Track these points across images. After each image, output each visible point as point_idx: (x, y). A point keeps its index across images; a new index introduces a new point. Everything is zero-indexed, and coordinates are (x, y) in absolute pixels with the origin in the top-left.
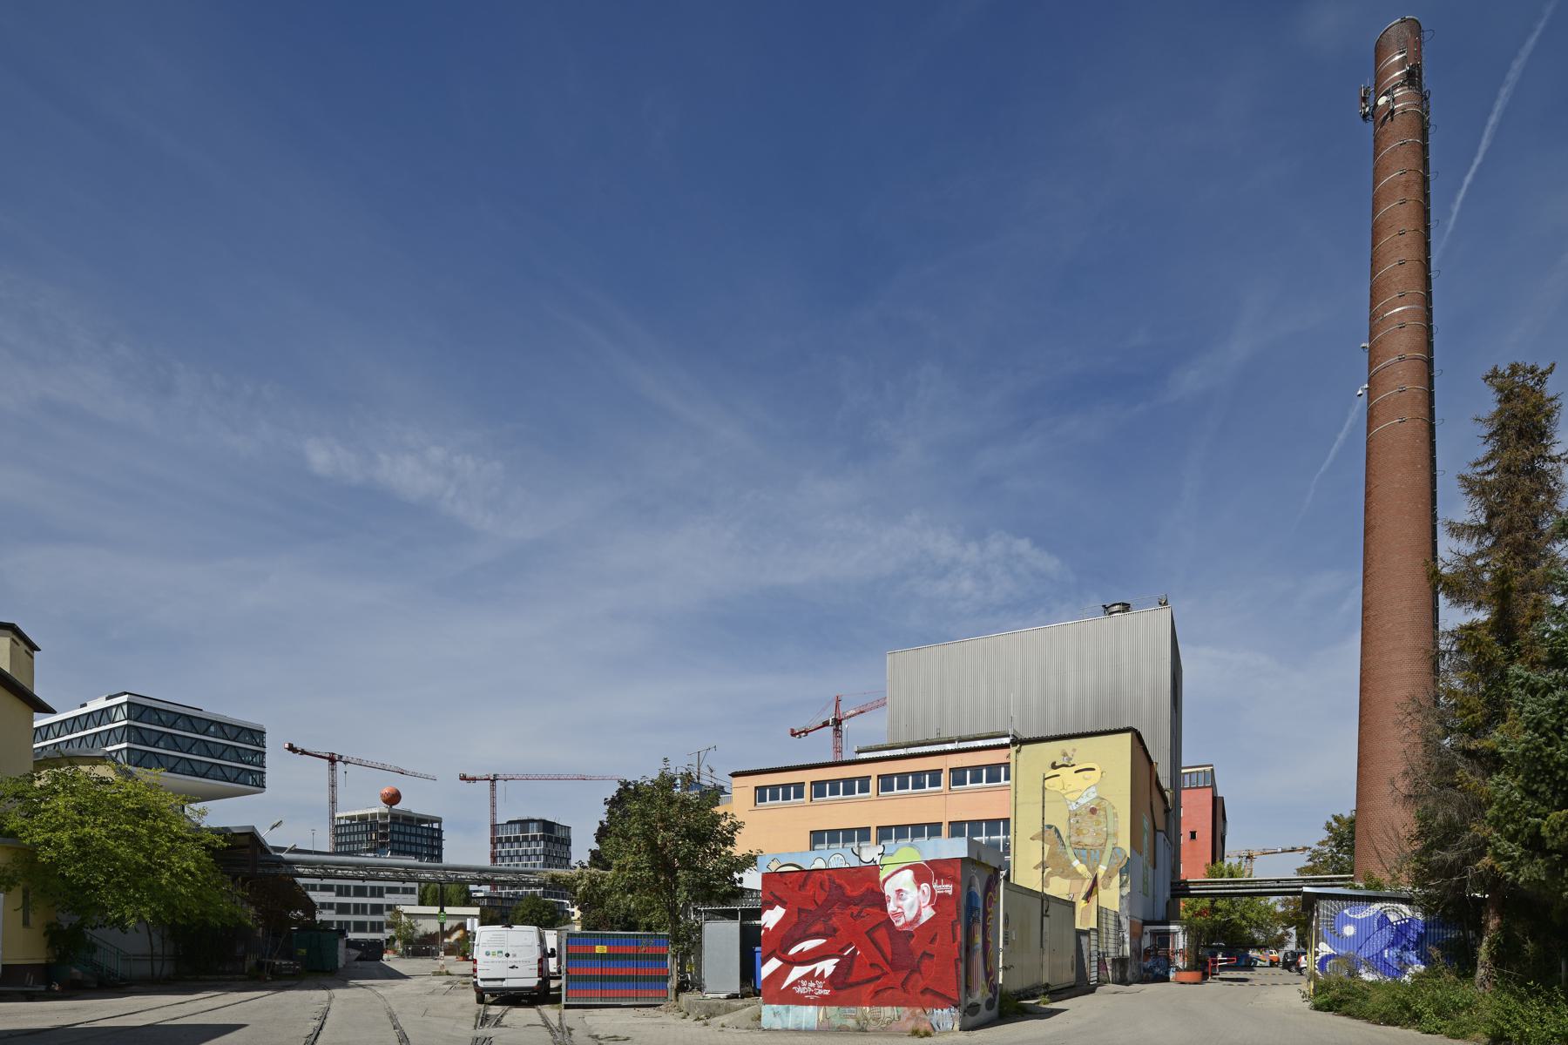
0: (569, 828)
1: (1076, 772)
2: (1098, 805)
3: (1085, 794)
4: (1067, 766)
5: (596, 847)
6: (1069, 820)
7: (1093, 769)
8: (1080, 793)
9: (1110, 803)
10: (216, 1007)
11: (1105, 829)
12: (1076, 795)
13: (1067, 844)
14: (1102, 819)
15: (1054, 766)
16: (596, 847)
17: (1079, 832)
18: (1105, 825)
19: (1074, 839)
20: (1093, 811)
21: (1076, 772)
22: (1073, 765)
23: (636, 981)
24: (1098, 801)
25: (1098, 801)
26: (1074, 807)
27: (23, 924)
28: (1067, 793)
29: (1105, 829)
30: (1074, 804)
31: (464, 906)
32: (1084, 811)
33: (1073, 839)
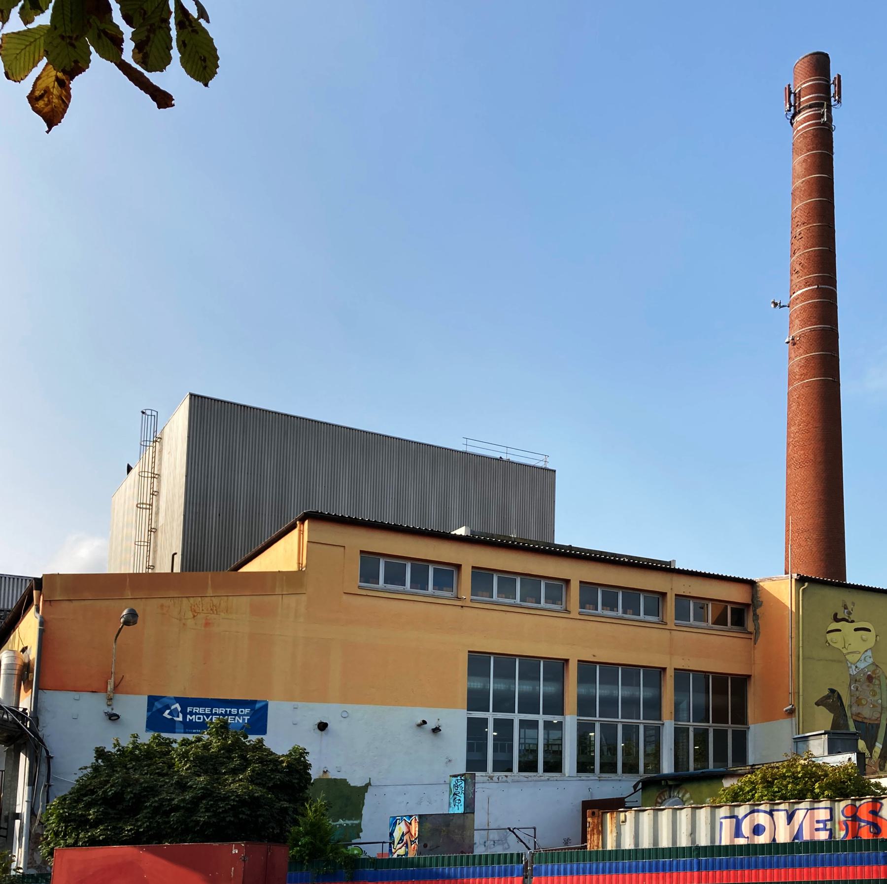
0: (555, 471)
1: (856, 630)
2: (874, 672)
3: (863, 658)
4: (847, 621)
5: (71, 82)
6: (850, 686)
7: (869, 630)
8: (859, 655)
9: (883, 672)
10: (696, 634)
11: (880, 701)
12: (856, 657)
13: (849, 714)
14: (878, 691)
15: (836, 619)
16: (71, 82)
17: (858, 702)
18: (879, 697)
19: (855, 709)
20: (870, 678)
21: (856, 630)
22: (853, 622)
23: (699, 869)
24: (873, 668)
25: (873, 668)
26: (853, 671)
27: (147, 726)
28: (848, 653)
29: (880, 701)
30: (854, 667)
31: (577, 763)
32: (863, 678)
33: (854, 709)
